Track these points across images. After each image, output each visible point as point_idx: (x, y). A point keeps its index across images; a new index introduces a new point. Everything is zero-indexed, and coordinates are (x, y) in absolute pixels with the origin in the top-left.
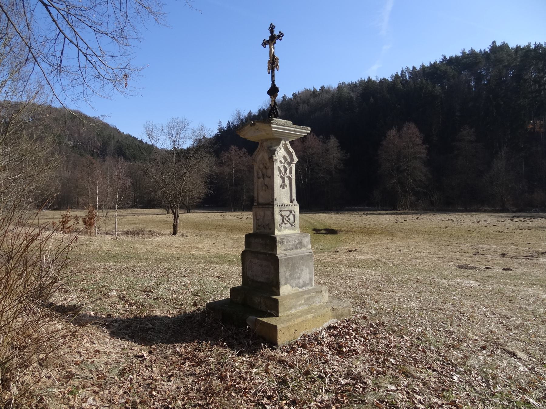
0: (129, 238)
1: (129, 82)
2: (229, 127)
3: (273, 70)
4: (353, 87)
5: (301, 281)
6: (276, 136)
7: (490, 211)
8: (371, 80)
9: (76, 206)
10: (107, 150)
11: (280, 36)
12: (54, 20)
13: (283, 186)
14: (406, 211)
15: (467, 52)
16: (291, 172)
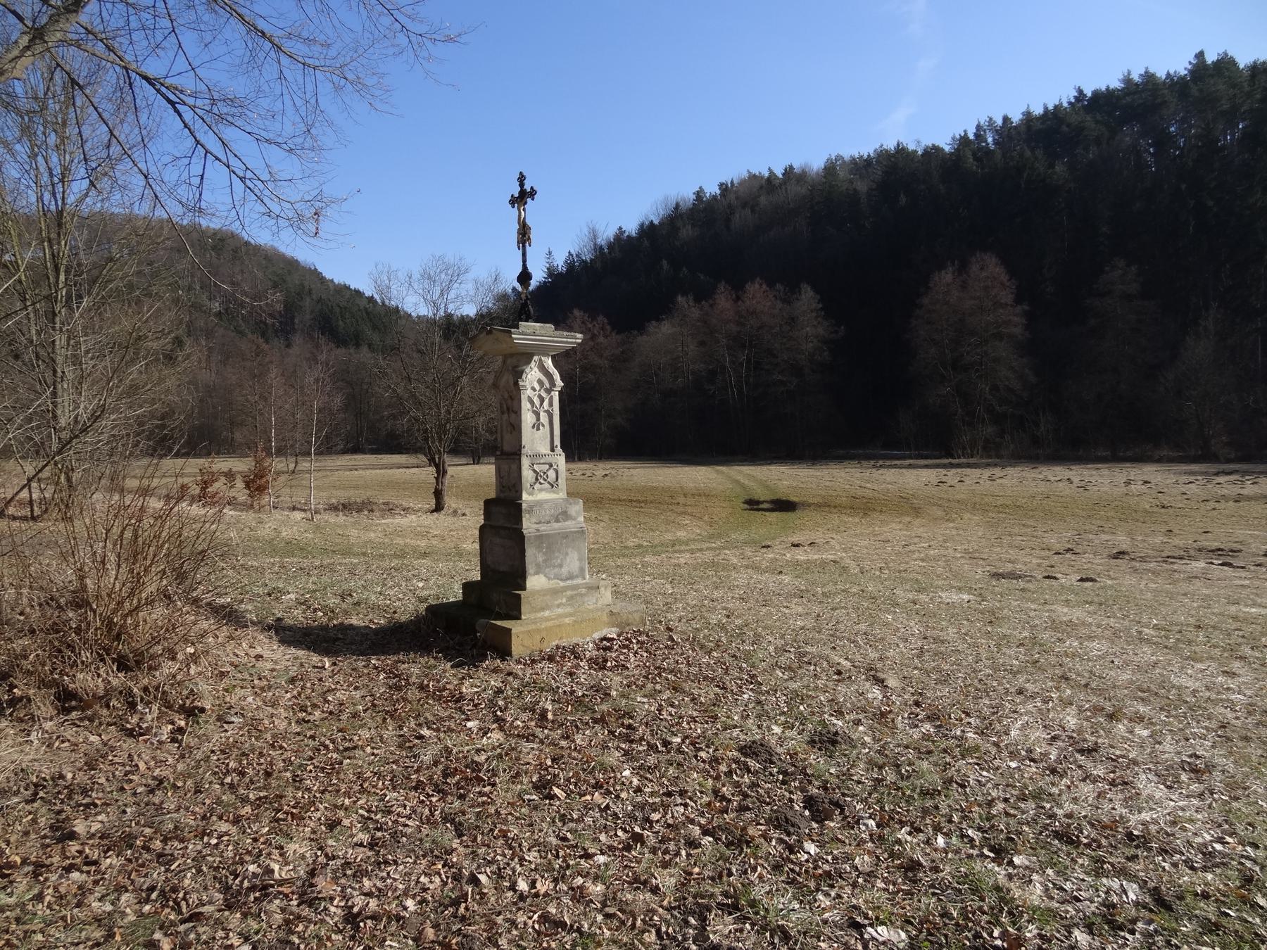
0: (341, 518)
1: (321, 225)
2: (570, 266)
3: (524, 246)
4: (861, 166)
5: (565, 571)
6: (523, 350)
7: (1171, 460)
8: (903, 149)
9: (228, 447)
10: (296, 321)
11: (532, 193)
12: (186, 126)
13: (537, 426)
14: (971, 461)
15: (1136, 77)
16: (551, 404)
